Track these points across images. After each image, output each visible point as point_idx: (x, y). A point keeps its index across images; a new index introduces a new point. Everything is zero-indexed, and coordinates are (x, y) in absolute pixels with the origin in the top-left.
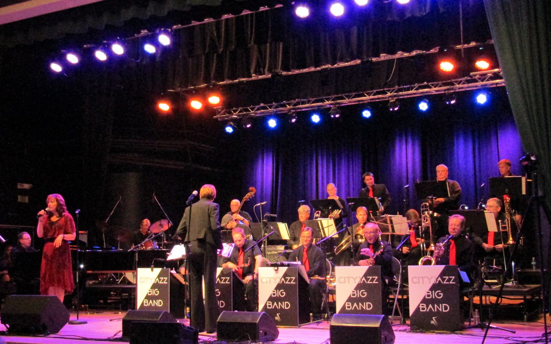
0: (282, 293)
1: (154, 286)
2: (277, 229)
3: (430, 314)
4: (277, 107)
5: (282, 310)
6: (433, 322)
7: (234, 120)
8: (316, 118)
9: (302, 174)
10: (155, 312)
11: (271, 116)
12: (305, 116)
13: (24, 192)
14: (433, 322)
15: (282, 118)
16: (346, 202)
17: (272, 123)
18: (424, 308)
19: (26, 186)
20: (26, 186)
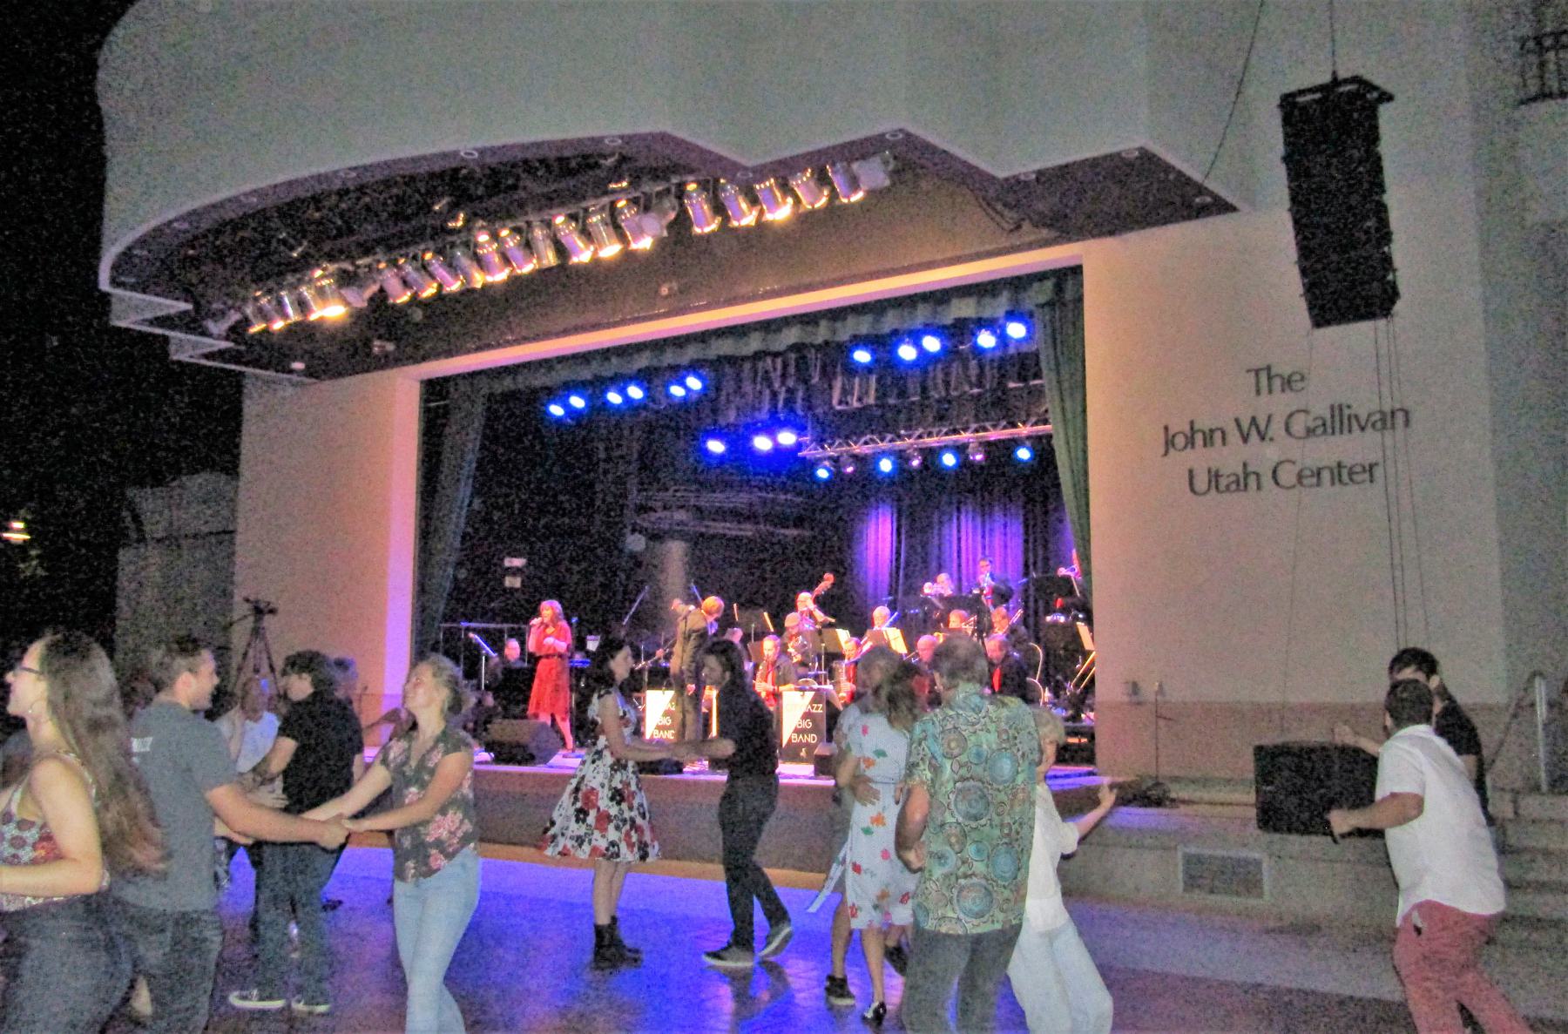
0: (808, 724)
1: (807, 715)
2: (836, 639)
3: (800, 745)
4: (977, 431)
5: (807, 745)
6: (803, 754)
7: (830, 458)
8: (949, 460)
9: (936, 552)
10: (660, 743)
11: (884, 454)
12: (931, 454)
13: (515, 572)
14: (803, 754)
15: (901, 457)
16: (1069, 600)
17: (886, 465)
18: (796, 739)
19: (518, 562)
20: (518, 562)
